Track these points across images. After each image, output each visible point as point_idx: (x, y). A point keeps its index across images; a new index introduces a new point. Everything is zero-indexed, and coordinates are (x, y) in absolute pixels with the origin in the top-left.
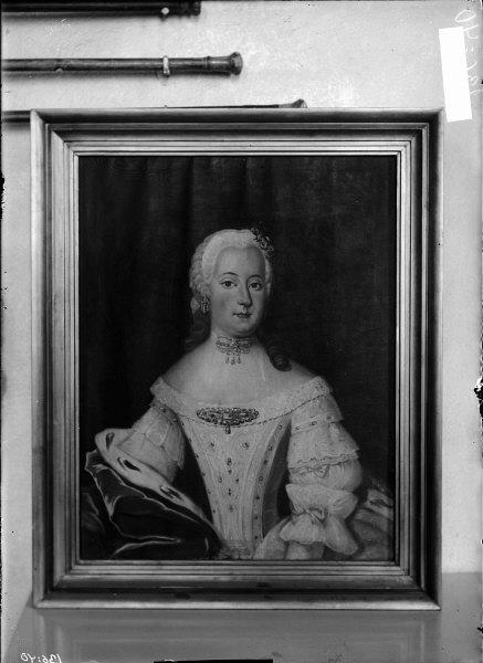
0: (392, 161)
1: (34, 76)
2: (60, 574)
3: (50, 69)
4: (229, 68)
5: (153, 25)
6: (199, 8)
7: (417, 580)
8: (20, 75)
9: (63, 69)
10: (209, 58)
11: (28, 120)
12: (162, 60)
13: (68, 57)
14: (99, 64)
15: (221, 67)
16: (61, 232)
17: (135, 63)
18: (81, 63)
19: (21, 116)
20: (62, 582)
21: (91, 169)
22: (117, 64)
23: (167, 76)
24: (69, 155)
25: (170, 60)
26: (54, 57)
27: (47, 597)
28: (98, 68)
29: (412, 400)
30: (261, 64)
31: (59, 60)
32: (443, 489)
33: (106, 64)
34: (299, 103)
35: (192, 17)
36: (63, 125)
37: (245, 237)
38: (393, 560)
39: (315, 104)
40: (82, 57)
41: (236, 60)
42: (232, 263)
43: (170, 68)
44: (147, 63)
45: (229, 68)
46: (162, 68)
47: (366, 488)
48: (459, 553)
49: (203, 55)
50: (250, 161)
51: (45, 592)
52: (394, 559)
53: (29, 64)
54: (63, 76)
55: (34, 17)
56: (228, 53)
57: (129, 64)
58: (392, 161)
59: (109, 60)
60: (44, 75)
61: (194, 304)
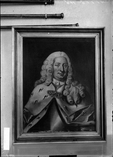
0: (94, 39)
2: (18, 137)
4: (61, 17)
5: (43, 6)
6: (54, 2)
7: (101, 135)
9: (22, 17)
10: (56, 14)
11: (11, 28)
12: (45, 15)
14: (31, 16)
15: (59, 16)
17: (39, 15)
18: (26, 15)
20: (19, 138)
21: (25, 40)
23: (46, 18)
24: (21, 37)
25: (47, 15)
27: (15, 142)
28: (30, 17)
29: (99, 87)
30: (68, 16)
31: (21, 15)
32: (107, 128)
33: (32, 16)
34: (77, 25)
35: (52, 5)
36: (19, 30)
37: (63, 54)
38: (95, 131)
41: (62, 15)
42: (59, 60)
44: (42, 15)
45: (61, 17)
48: (110, 132)
49: (55, 13)
51: (15, 141)
52: (95, 130)
54: (22, 18)
55: (15, 5)
56: (61, 13)
57: (37, 16)
58: (94, 39)
59: (33, 15)
60: (18, 18)
61: (32, 93)
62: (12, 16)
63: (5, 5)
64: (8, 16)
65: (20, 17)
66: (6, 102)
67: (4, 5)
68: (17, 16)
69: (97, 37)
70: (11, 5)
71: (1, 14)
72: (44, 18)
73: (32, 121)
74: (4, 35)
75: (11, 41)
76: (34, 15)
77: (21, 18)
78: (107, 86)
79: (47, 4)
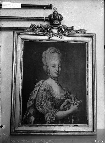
1: (16, 20)
12: (44, 18)
18: (27, 18)
22: (34, 18)
28: (30, 19)
46: (44, 19)
54: (23, 20)
76: (34, 17)
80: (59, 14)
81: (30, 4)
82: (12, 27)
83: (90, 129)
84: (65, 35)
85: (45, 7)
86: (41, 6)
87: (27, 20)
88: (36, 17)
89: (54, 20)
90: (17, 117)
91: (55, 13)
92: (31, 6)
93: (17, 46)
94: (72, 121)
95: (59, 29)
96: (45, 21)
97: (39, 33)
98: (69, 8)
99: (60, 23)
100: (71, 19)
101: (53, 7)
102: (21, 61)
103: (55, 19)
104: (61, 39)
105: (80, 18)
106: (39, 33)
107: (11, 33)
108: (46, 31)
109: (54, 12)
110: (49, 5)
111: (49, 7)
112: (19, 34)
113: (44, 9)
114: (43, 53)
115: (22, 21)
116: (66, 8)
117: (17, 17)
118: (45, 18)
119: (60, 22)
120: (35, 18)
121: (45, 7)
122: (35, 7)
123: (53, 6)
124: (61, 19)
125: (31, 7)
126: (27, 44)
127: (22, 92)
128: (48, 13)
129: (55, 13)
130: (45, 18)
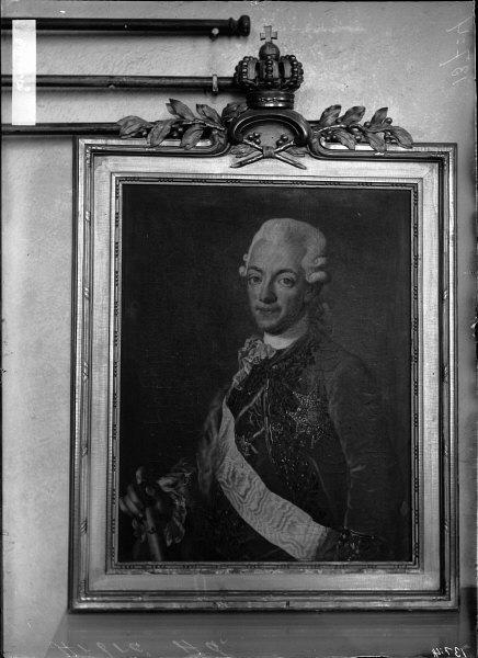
0: (401, 200)
1: (86, 92)
3: (103, 86)
6: (248, 28)
8: (73, 91)
12: (211, 78)
13: (120, 74)
14: (150, 81)
16: (100, 245)
18: (132, 80)
19: (73, 128)
22: (168, 82)
26: (108, 74)
28: (149, 86)
33: (157, 81)
39: (437, 357)
40: (133, 74)
43: (219, 86)
44: (197, 81)
46: (211, 86)
47: (308, 284)
50: (272, 248)
53: (82, 80)
54: (115, 92)
55: (88, 36)
58: (401, 200)
60: (96, 91)
62: (73, 81)
63: (63, 36)
64: (59, 80)
65: (108, 86)
66: (41, 441)
67: (54, 35)
68: (93, 80)
69: (89, 141)
70: (70, 35)
71: (3, 73)
72: (205, 93)
73: (162, 502)
74: (39, 160)
75: (248, 190)
76: (166, 77)
77: (112, 90)
78: (18, 546)
79: (213, 27)
80: (290, 59)
81: (148, 17)
82: (64, 121)
83: (430, 581)
84: (317, 155)
85: (216, 31)
86: (201, 24)
87: (136, 92)
88: (178, 74)
89: (261, 97)
90: (99, 411)
91: (268, 56)
92: (152, 24)
93: (90, 197)
94: (278, 482)
95: (290, 122)
96: (215, 95)
97: (199, 144)
98: (329, 34)
99: (289, 103)
100: (339, 82)
101: (257, 28)
102: (112, 330)
103: (265, 83)
104: (304, 173)
105: (379, 81)
106: (199, 144)
107: (63, 152)
108: (230, 136)
109: (263, 49)
110: (236, 18)
111: (237, 29)
112: (98, 152)
113: (213, 38)
114: (265, 220)
115: (111, 94)
116: (316, 31)
117: (88, 79)
118: (215, 79)
119: (293, 96)
120: (172, 81)
121: (216, 31)
122: (164, 28)
123: (252, 25)
124: (292, 83)
125: (153, 28)
126: (138, 199)
127: (118, 434)
128: (226, 59)
129: (268, 56)
130: (215, 79)
